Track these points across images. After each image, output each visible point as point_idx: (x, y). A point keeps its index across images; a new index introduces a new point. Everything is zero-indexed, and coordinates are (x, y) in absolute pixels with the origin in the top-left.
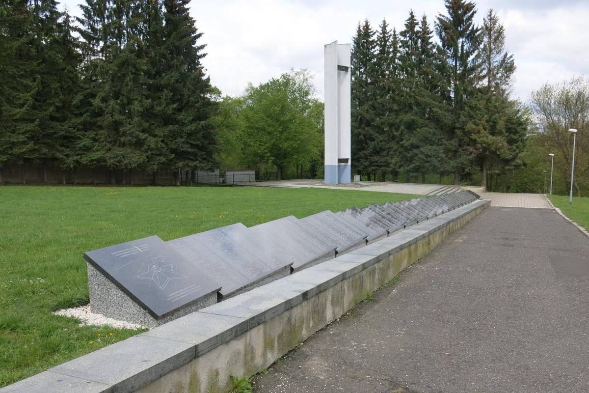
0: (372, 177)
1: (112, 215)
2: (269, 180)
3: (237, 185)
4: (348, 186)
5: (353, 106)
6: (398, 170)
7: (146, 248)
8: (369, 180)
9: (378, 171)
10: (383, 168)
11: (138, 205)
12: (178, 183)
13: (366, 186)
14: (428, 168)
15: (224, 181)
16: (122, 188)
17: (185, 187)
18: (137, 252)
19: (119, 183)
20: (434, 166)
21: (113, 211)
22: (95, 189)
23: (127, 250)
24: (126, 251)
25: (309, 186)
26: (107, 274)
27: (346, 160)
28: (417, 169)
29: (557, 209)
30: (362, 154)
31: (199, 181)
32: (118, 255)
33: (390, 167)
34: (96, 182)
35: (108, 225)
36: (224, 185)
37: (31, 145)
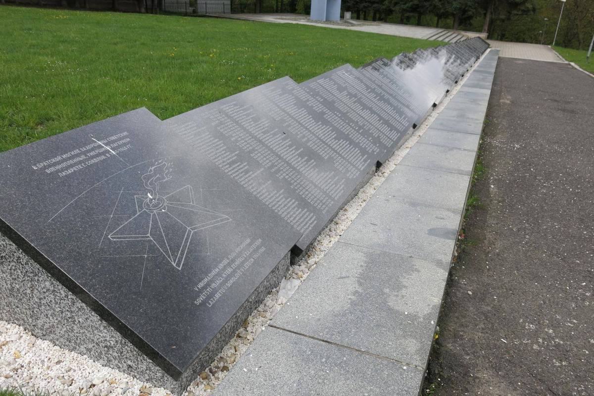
0: (362, 16)
1: (61, 47)
2: (242, 12)
3: (211, 17)
4: (338, 24)
6: (393, 9)
7: (125, 144)
8: (358, 18)
9: (370, 9)
10: (375, 5)
11: (97, 33)
13: (358, 25)
14: (428, 8)
15: (194, 11)
16: (75, 12)
17: (151, 15)
18: (103, 157)
20: (435, 6)
21: (63, 42)
22: (40, 10)
23: (77, 151)
24: (72, 157)
25: (294, 22)
28: (414, 9)
29: (572, 64)
31: (167, 9)
32: (52, 169)
33: (384, 5)
34: (43, 3)
35: (53, 62)
36: (195, 15)
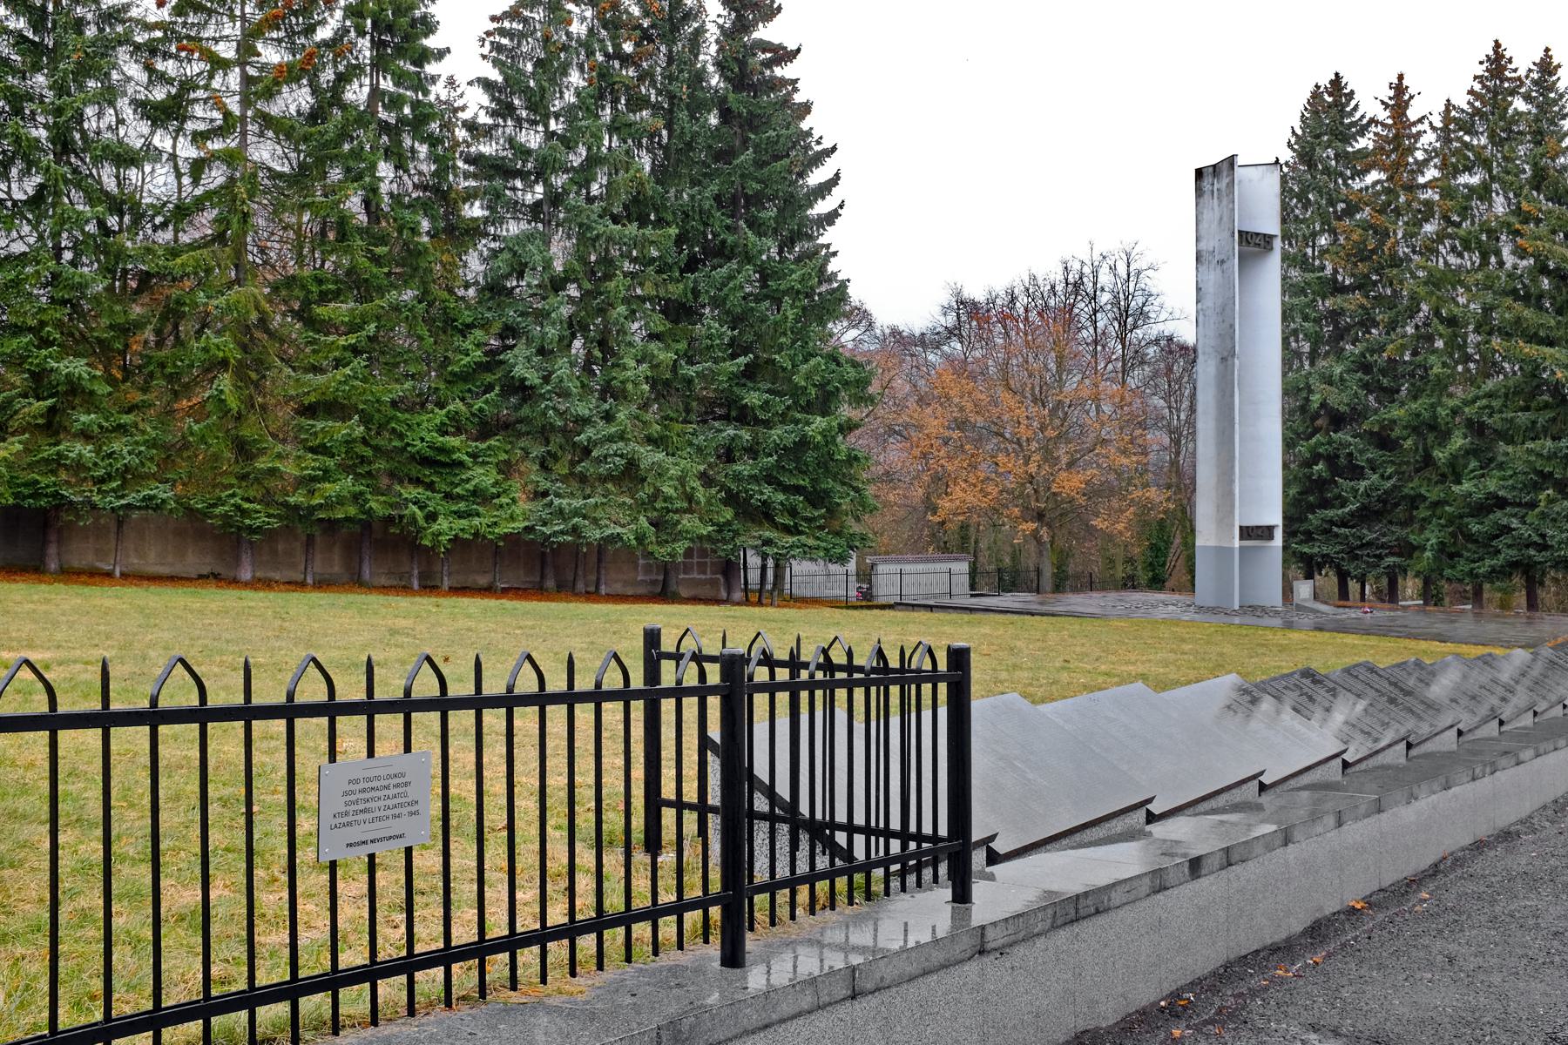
5: (1290, 357)
12: (738, 595)
19: (566, 589)
26: (56, 742)
27: (1266, 532)
30: (1314, 519)
37: (345, 484)
